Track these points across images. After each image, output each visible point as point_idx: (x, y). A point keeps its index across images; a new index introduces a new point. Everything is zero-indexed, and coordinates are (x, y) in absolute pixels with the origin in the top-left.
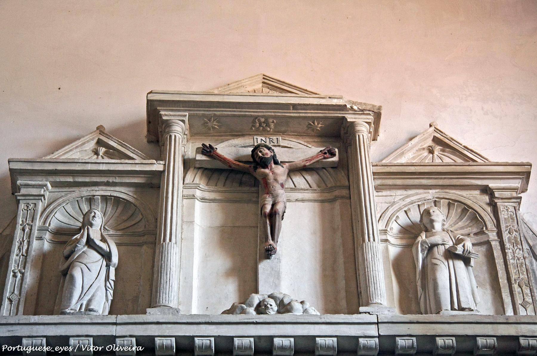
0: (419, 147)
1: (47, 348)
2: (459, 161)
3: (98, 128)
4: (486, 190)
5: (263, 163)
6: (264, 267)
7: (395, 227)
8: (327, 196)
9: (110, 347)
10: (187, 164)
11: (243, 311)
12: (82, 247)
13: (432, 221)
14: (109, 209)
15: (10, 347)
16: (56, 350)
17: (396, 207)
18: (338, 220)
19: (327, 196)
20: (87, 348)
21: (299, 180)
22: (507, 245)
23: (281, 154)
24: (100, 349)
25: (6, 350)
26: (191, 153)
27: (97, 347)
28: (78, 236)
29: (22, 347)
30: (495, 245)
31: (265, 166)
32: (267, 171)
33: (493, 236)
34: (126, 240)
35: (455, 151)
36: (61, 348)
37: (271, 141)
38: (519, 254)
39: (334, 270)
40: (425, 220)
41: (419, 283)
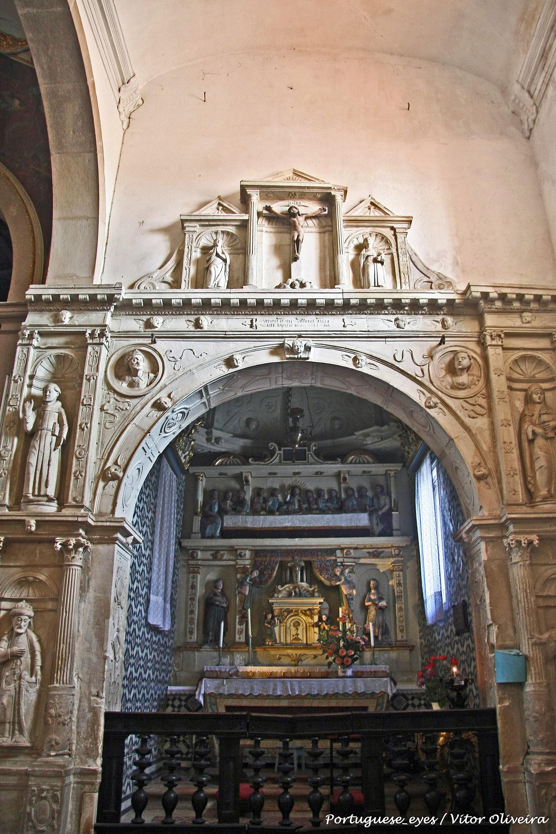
0: (364, 206)
1: (396, 820)
2: (382, 214)
3: (218, 197)
4: (392, 228)
5: (294, 215)
6: (294, 265)
7: (352, 246)
8: (322, 230)
9: (496, 817)
10: (259, 214)
11: (285, 287)
12: (214, 257)
13: (368, 244)
14: (225, 236)
15: (339, 817)
16: (411, 823)
17: (353, 236)
18: (327, 243)
19: (322, 230)
20: (459, 819)
21: (309, 221)
22: (400, 255)
23: (302, 210)
24: (480, 820)
25: (332, 822)
26: (261, 209)
27: (474, 817)
28: (212, 251)
29: (357, 818)
30: (395, 255)
31: (295, 217)
32: (295, 219)
33: (394, 250)
34: (232, 251)
35: (380, 209)
36: (418, 819)
37: (297, 203)
38: (405, 259)
39: (324, 266)
40: (365, 243)
41: (361, 274)
